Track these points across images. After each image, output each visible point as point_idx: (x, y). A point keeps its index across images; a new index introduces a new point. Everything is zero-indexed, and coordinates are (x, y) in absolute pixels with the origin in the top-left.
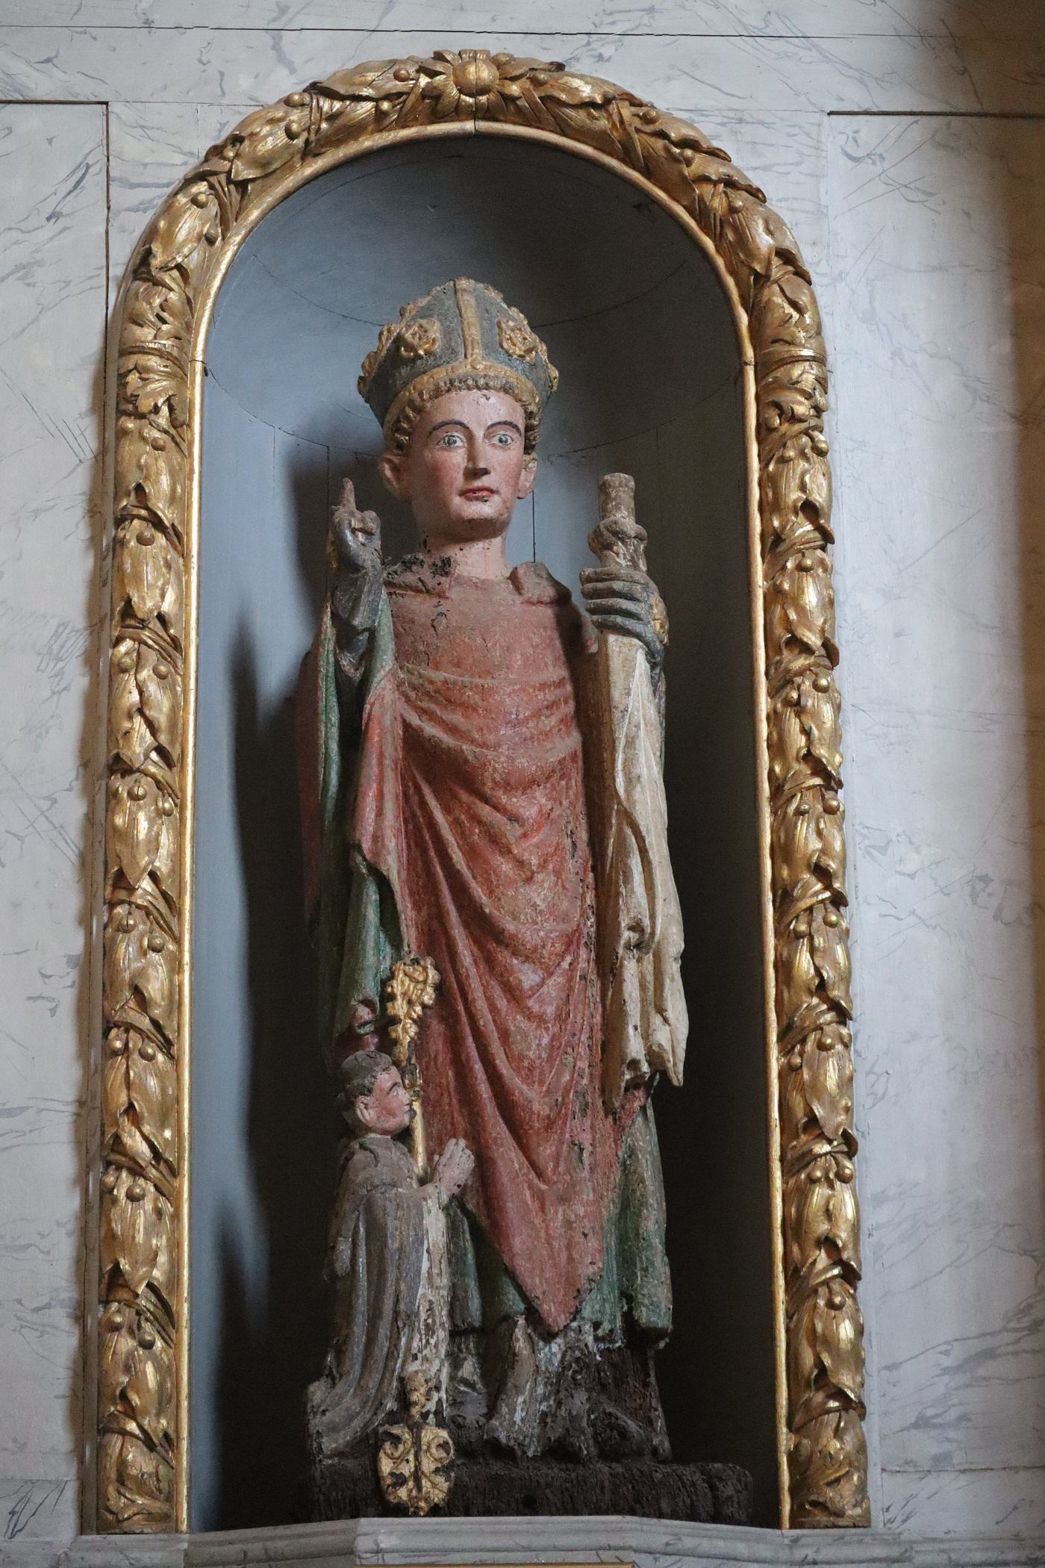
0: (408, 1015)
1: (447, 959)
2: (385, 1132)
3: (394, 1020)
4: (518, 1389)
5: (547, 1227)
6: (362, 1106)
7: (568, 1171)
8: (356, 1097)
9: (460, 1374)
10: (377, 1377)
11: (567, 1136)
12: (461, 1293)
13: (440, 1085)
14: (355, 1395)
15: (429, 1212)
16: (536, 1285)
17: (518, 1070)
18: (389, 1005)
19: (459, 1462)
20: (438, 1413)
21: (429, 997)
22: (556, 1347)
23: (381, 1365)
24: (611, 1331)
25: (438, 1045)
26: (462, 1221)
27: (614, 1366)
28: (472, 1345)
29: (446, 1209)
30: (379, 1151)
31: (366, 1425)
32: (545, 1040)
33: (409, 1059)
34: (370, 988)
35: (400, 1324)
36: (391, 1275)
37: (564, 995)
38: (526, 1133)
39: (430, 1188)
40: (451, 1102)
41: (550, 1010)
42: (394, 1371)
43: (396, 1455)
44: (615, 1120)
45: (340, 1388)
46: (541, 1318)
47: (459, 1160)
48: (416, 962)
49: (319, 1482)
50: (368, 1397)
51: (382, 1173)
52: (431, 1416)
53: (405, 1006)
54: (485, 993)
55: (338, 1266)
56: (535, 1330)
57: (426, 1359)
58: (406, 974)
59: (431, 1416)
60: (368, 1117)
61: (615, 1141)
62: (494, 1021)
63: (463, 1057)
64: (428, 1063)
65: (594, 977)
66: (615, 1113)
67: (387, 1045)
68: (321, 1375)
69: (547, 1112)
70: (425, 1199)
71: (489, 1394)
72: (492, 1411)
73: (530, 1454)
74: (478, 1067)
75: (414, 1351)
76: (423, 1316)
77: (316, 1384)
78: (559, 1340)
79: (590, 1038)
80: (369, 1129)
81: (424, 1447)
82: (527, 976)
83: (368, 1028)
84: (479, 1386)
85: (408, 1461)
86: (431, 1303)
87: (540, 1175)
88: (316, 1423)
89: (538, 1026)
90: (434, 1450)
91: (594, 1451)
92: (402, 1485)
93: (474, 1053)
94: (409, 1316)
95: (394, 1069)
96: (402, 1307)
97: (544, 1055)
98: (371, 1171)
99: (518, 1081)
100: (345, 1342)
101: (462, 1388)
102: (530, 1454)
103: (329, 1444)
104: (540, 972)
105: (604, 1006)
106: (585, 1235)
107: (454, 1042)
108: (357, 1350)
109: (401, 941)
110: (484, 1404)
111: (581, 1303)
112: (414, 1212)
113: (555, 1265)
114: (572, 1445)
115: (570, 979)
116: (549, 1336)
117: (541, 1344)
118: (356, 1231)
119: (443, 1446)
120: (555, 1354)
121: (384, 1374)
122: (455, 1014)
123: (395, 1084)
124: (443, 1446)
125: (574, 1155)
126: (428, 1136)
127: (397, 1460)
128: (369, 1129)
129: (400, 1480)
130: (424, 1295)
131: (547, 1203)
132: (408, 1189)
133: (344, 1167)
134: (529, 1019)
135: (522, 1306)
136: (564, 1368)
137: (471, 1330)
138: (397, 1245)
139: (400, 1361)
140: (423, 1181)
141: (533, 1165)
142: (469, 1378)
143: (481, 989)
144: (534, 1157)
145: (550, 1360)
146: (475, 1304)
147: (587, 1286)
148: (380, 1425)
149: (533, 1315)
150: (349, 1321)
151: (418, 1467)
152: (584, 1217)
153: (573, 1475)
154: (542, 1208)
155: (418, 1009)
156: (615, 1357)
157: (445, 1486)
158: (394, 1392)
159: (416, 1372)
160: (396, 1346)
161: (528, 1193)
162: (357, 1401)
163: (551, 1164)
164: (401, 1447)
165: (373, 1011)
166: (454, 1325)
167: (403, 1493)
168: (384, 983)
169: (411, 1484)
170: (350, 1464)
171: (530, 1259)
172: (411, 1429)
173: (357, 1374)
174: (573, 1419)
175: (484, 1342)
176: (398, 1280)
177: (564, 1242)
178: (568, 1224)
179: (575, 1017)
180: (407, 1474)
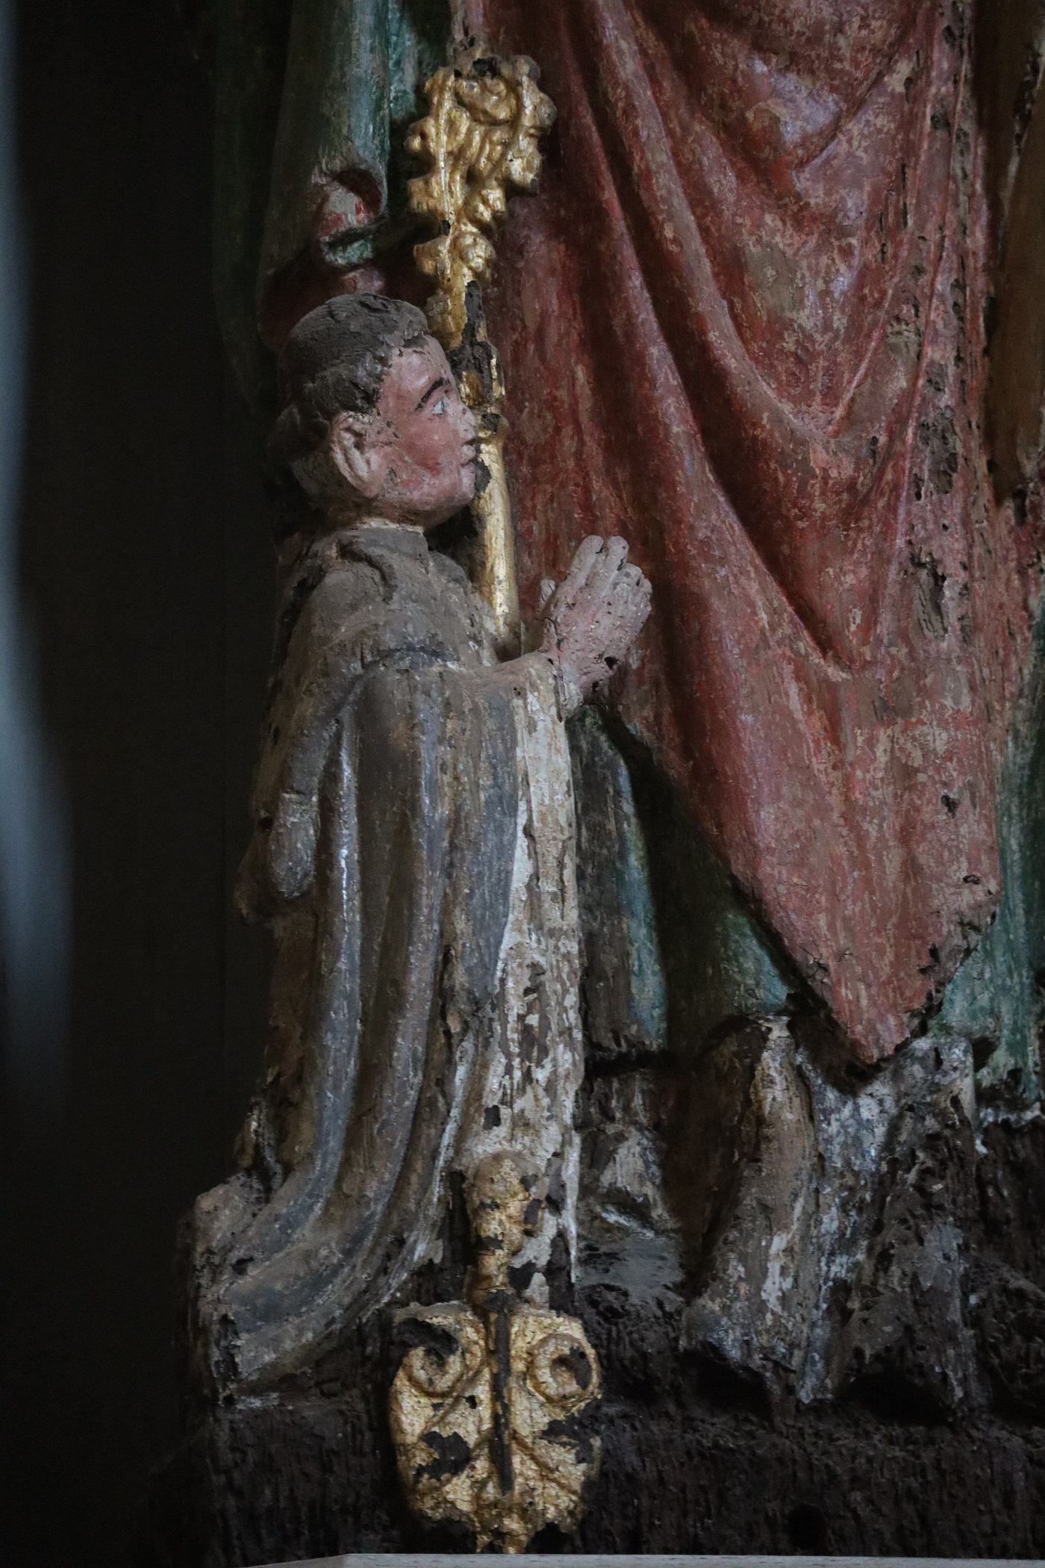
0: (468, 212)
1: (572, 64)
2: (409, 514)
3: (432, 226)
4: (771, 1217)
5: (848, 783)
6: (349, 439)
7: (903, 635)
8: (330, 415)
9: (606, 1178)
10: (388, 1172)
11: (900, 542)
12: (609, 960)
13: (552, 404)
14: (327, 1216)
15: (532, 727)
16: (820, 931)
17: (766, 361)
18: (416, 185)
19: (612, 1410)
20: (555, 1271)
21: (523, 166)
22: (873, 1105)
23: (401, 1135)
24: (1015, 1074)
25: (546, 298)
26: (611, 766)
27: (1018, 1170)
28: (638, 1101)
29: (573, 725)
30: (397, 563)
31: (359, 1303)
32: (843, 282)
33: (470, 330)
34: (363, 140)
35: (455, 1026)
36: (428, 897)
37: (892, 167)
38: (789, 526)
39: (532, 665)
40: (584, 445)
41: (854, 203)
42: (434, 1155)
43: (443, 1383)
44: (1021, 513)
45: (286, 1197)
46: (834, 1024)
47: (608, 597)
48: (487, 69)
49: (227, 1458)
50: (366, 1223)
51: (404, 620)
52: (538, 1278)
53: (458, 188)
54: (676, 154)
55: (280, 869)
56: (814, 1059)
57: (521, 1123)
58: (460, 101)
59: (538, 1278)
60: (363, 471)
61: (1022, 572)
62: (704, 231)
63: (617, 324)
64: (518, 347)
65: (968, 126)
66: (1020, 495)
67: (407, 278)
68: (232, 1168)
69: (848, 470)
70: (520, 693)
71: (686, 1233)
72: (698, 1272)
73: (805, 1396)
74: (658, 353)
75: (491, 1101)
76: (515, 1006)
77: (220, 1190)
78: (881, 1088)
79: (959, 285)
80: (367, 505)
81: (519, 1366)
82: (796, 110)
83: (356, 252)
84: (659, 1212)
85: (473, 1402)
86: (536, 970)
87: (826, 642)
88: (221, 1295)
89: (823, 247)
90: (545, 1374)
91: (980, 1398)
92: (456, 1469)
93: (646, 316)
94: (477, 1004)
95: (433, 345)
96: (460, 977)
97: (839, 321)
98: (372, 613)
99: (767, 390)
100: (299, 1079)
101: (613, 1218)
102: (805, 1396)
103: (254, 1354)
104: (831, 99)
105: (995, 205)
106: (950, 805)
107: (593, 289)
108: (332, 1098)
109: (447, 17)
110: (673, 1259)
111: (941, 985)
112: (490, 725)
113: (867, 882)
114: (922, 1371)
115: (908, 123)
116: (853, 1076)
117: (831, 1095)
118: (331, 776)
119: (570, 1363)
120: (869, 1126)
121: (407, 1164)
122: (597, 215)
123: (437, 384)
124: (570, 1363)
125: (919, 595)
126: (520, 540)
127: (445, 1400)
128: (367, 505)
129: (452, 1456)
130: (518, 949)
131: (847, 717)
132: (470, 666)
133: (296, 610)
134: (798, 225)
135: (780, 992)
136: (894, 1163)
137: (638, 1060)
138: (444, 810)
139: (451, 1128)
140: (506, 653)
141: (808, 615)
142: (633, 1188)
143: (666, 144)
144: (812, 593)
145: (857, 1141)
146: (648, 987)
147: (958, 940)
148: (394, 1303)
149: (811, 1015)
150: (312, 1017)
151: (501, 1419)
152: (949, 756)
153: (928, 1456)
154: (834, 731)
155: (495, 195)
156: (1023, 1149)
157: (575, 1473)
158: (434, 1212)
159: (497, 1158)
160: (443, 1083)
161: (793, 689)
162: (334, 1234)
163: (858, 615)
164: (455, 1364)
165: (370, 201)
166: (591, 1044)
167: (459, 1491)
168: (399, 131)
169: (482, 1466)
170: (311, 1409)
171: (800, 864)
172: (481, 1313)
173: (333, 1162)
174: (923, 1299)
175: (679, 1085)
176: (446, 912)
177: (892, 823)
178: (904, 774)
179: (921, 226)
180: (472, 1439)
